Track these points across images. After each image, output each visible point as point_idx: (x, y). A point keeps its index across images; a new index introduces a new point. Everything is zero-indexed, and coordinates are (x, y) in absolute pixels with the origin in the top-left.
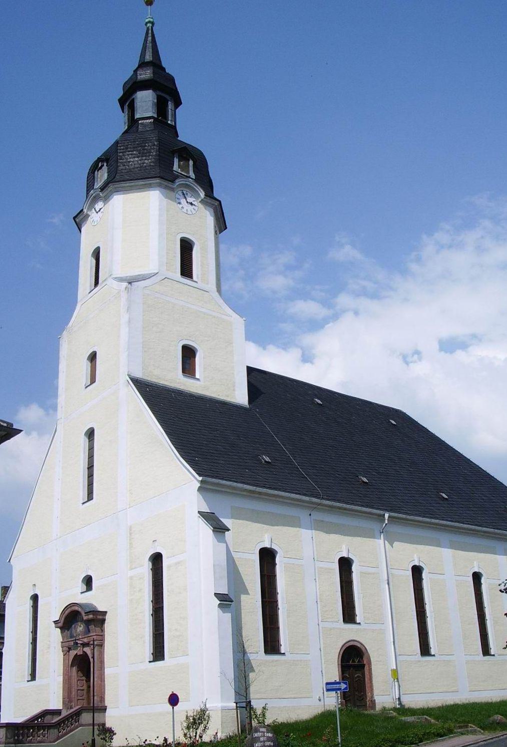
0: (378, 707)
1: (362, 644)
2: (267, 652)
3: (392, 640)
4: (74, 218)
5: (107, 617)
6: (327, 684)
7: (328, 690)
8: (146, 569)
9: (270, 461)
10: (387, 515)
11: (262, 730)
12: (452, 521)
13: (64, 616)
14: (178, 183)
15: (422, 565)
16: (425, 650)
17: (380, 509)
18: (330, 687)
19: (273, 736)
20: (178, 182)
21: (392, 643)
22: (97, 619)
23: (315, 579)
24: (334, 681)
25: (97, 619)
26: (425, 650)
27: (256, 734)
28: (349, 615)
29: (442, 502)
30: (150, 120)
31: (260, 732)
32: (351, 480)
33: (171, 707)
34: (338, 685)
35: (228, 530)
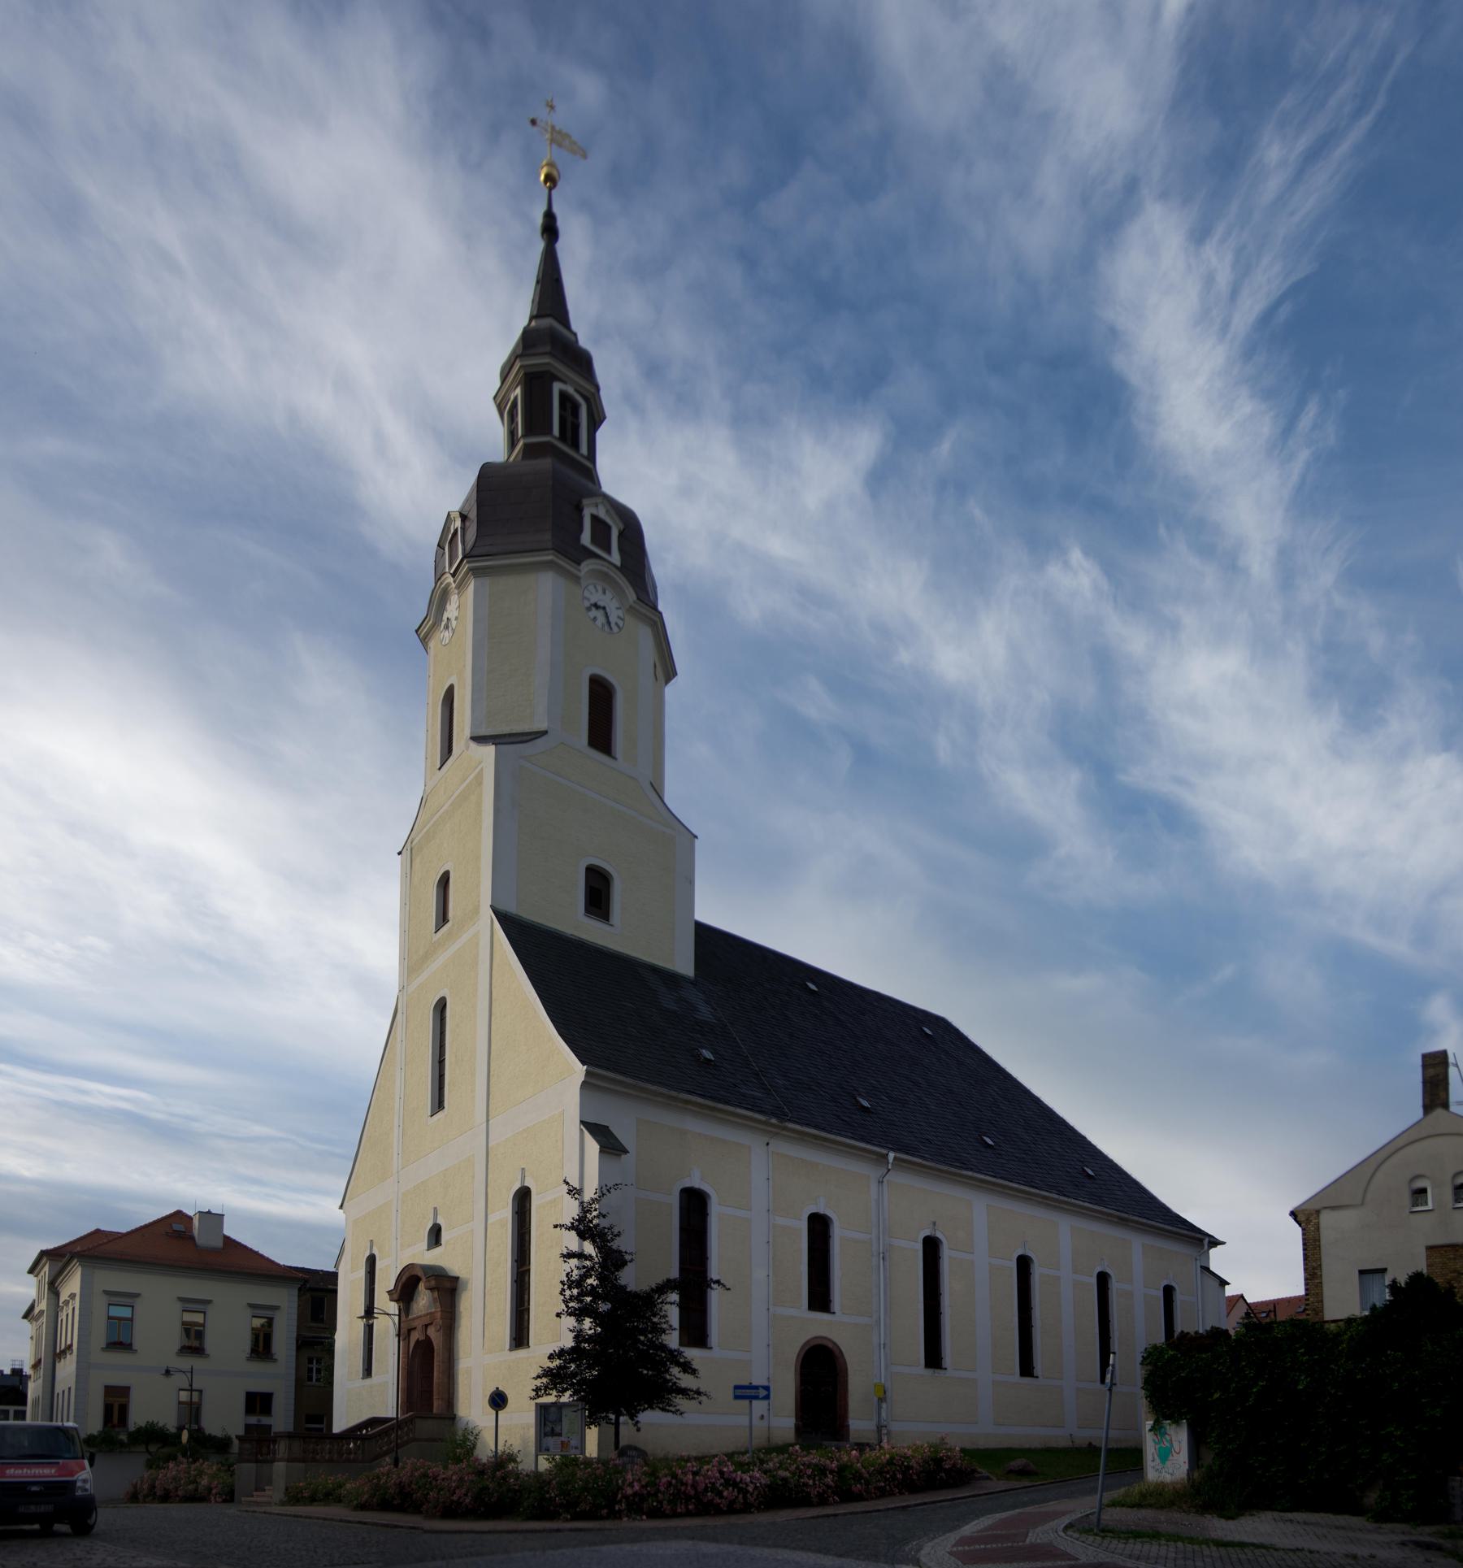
4: (417, 631)
6: (736, 1387)
7: (737, 1397)
8: (504, 1214)
9: (713, 1059)
10: (891, 1155)
12: (995, 1177)
13: (400, 1284)
14: (591, 567)
16: (933, 1357)
17: (883, 1147)
18: (739, 1392)
20: (587, 566)
22: (447, 1287)
23: (768, 1242)
24: (747, 1384)
25: (447, 1287)
26: (933, 1357)
28: (820, 1298)
29: (983, 1149)
32: (842, 1101)
33: (494, 1412)
34: (755, 1391)
35: (626, 1152)
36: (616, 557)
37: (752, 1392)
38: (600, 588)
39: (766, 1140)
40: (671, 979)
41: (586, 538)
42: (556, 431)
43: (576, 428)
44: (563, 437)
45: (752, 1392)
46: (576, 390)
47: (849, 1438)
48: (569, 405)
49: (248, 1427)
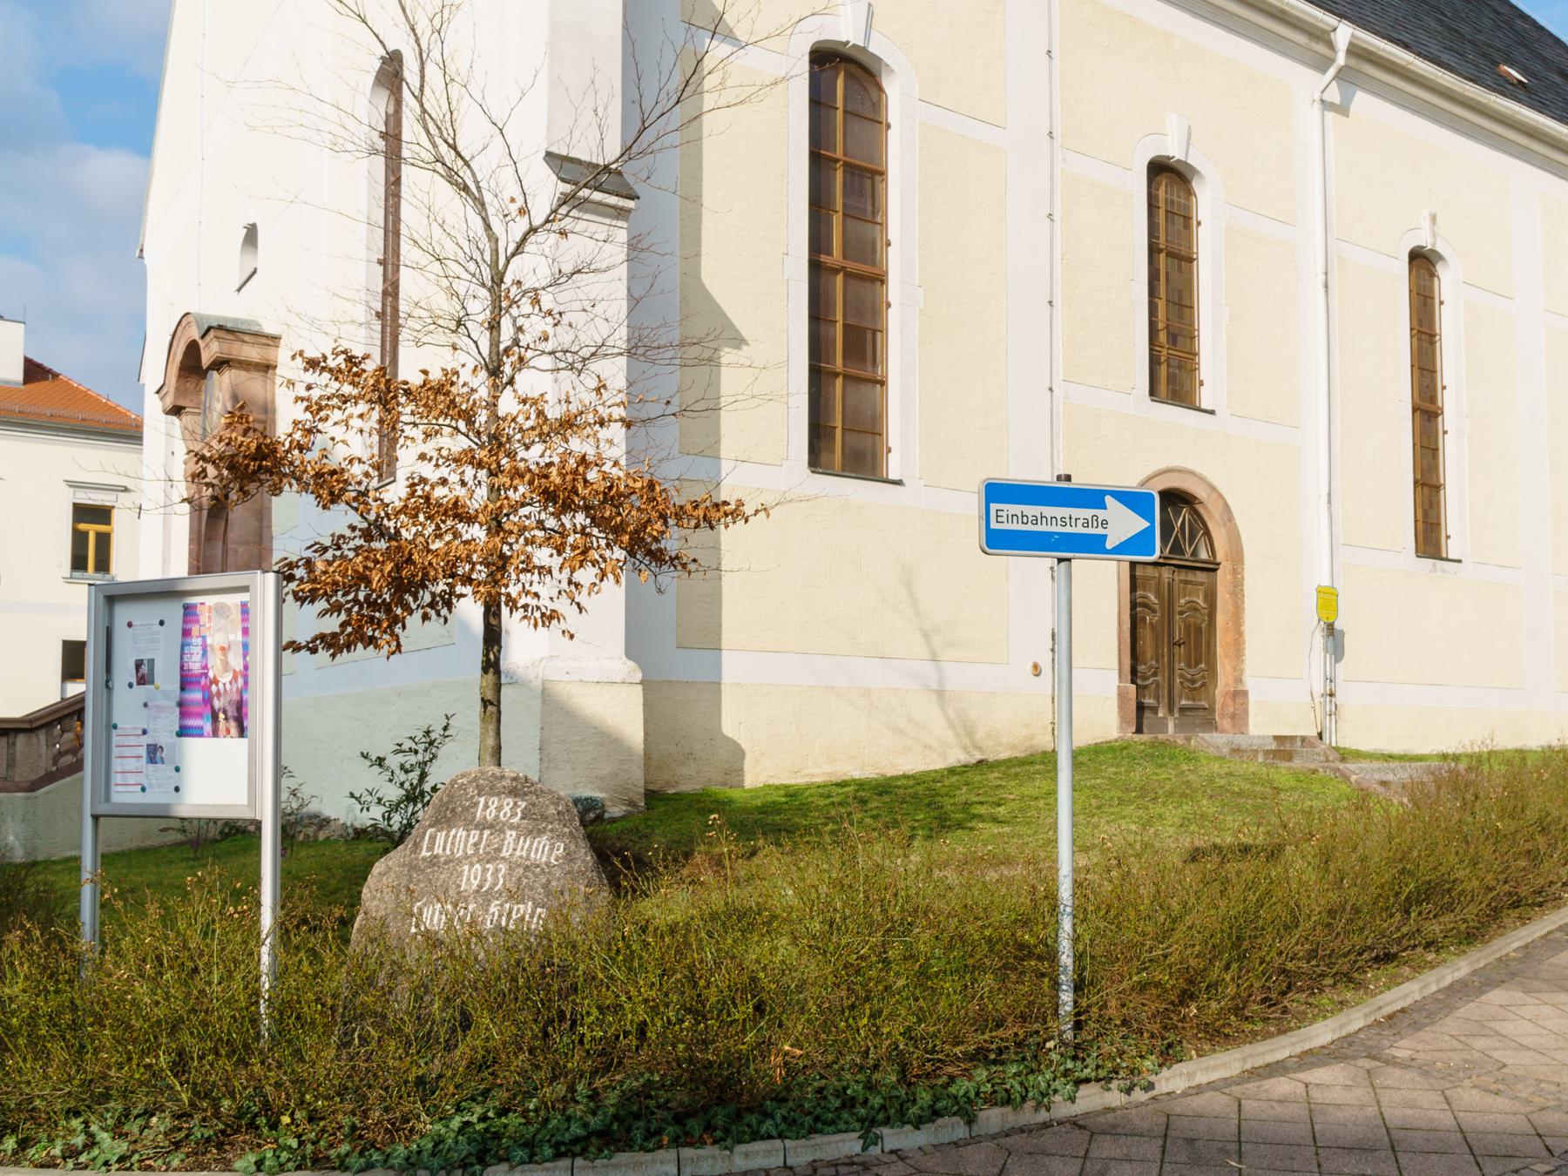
0: (1262, 725)
1: (1214, 489)
3: (1325, 490)
6: (997, 492)
7: (997, 541)
11: (490, 808)
16: (1429, 539)
18: (1012, 516)
19: (569, 857)
21: (1325, 499)
26: (1429, 539)
27: (441, 837)
30: (1091, 1099)
31: (471, 824)
34: (1087, 513)
37: (1076, 520)
45: (1076, 520)
47: (1246, 724)
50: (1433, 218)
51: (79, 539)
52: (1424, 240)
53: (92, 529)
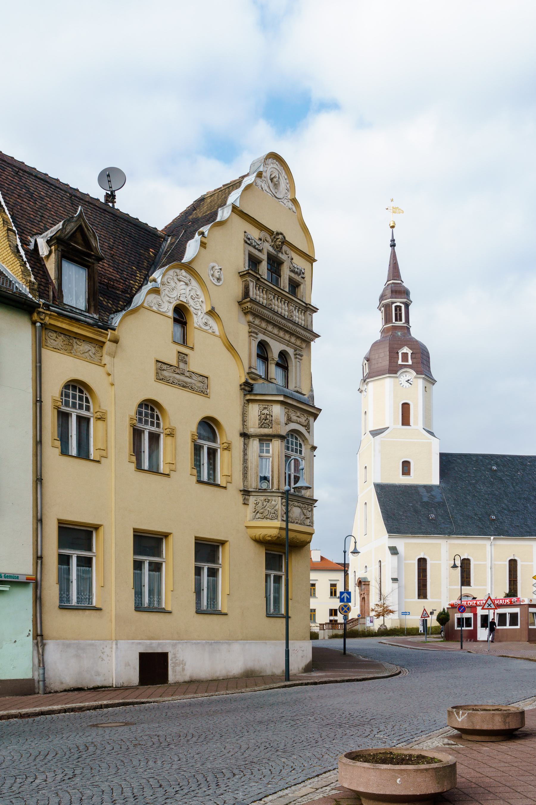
2: (420, 596)
5: (370, 583)
15: (516, 558)
36: (410, 362)
38: (404, 376)
39: (446, 540)
40: (428, 488)
41: (400, 362)
42: (394, 321)
43: (401, 314)
44: (396, 320)
46: (400, 303)
48: (398, 309)
49: (331, 621)
50: (514, 555)
51: (331, 589)
52: (512, 558)
53: (333, 588)
